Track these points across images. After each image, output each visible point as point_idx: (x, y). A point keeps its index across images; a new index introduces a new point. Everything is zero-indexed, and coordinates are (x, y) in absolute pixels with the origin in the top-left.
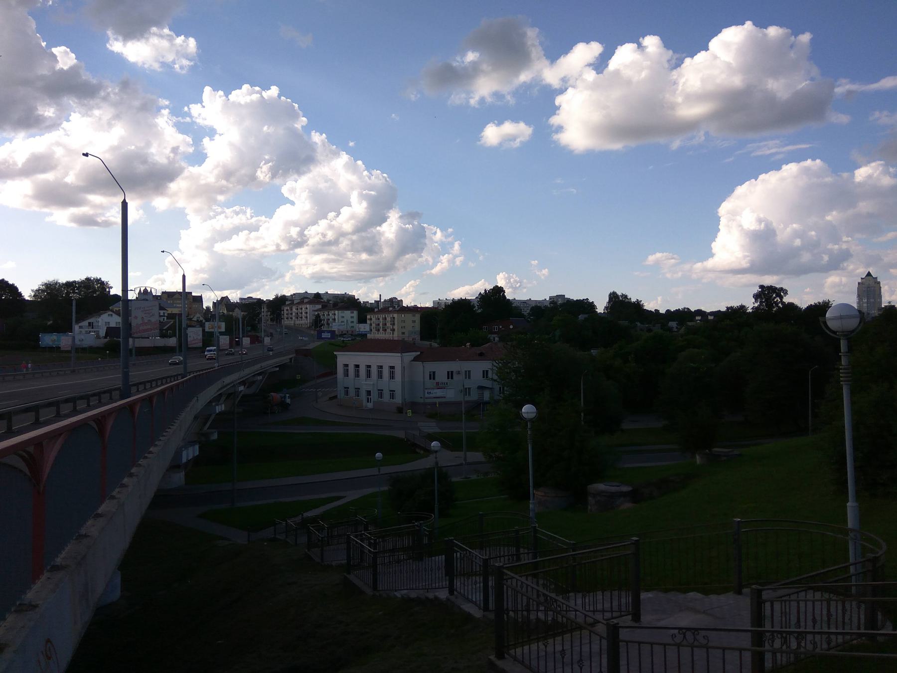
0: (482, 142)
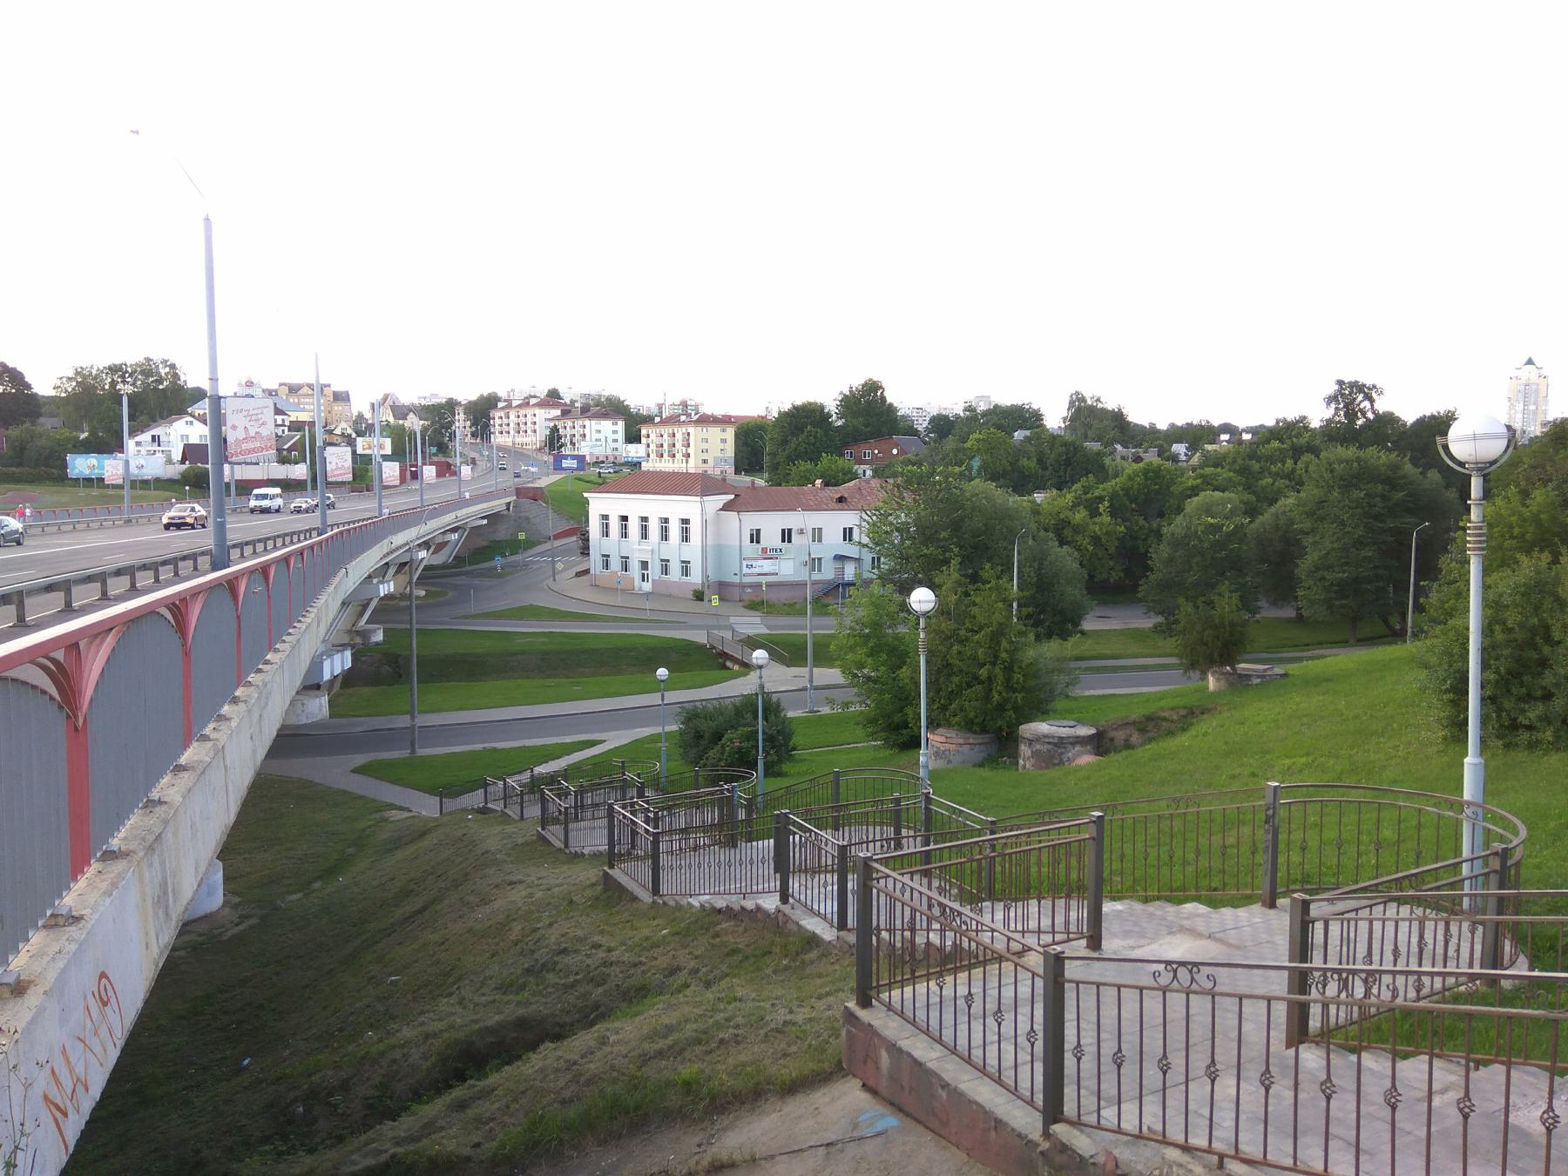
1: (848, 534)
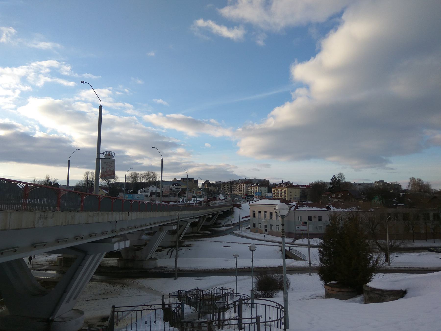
0: (296, 61)
1: (296, 192)
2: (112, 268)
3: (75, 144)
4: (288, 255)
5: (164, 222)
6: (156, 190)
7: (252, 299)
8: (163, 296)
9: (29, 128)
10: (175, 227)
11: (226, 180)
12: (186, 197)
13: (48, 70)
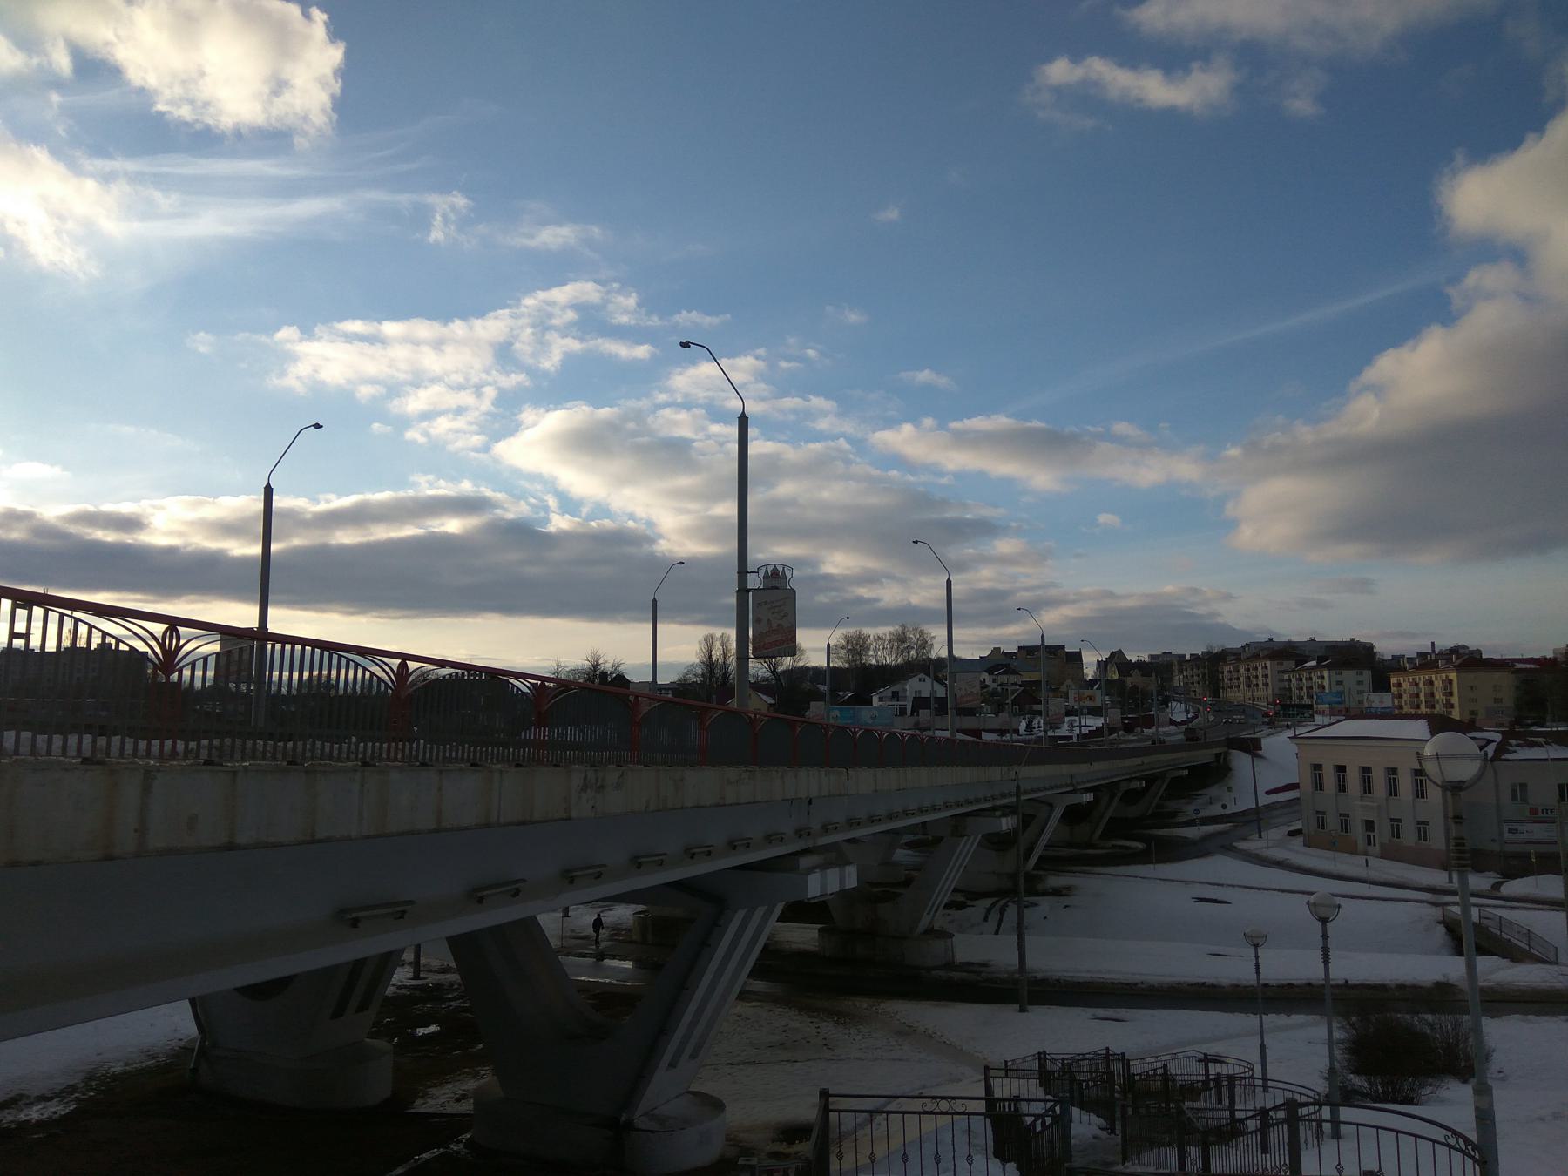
0: (1460, 159)
2: (803, 955)
3: (663, 547)
4: (1489, 943)
5: (968, 803)
6: (933, 692)
7: (1335, 1106)
8: (987, 1068)
9: (529, 504)
10: (1007, 824)
11: (1190, 648)
12: (1039, 713)
13: (571, 315)
